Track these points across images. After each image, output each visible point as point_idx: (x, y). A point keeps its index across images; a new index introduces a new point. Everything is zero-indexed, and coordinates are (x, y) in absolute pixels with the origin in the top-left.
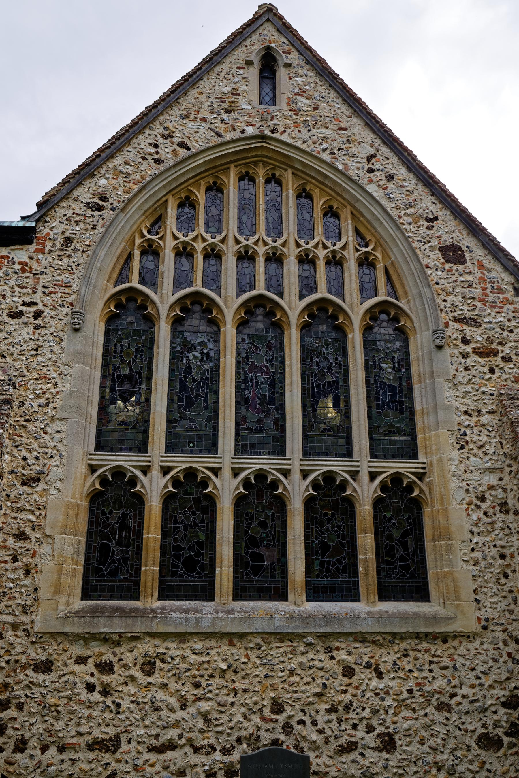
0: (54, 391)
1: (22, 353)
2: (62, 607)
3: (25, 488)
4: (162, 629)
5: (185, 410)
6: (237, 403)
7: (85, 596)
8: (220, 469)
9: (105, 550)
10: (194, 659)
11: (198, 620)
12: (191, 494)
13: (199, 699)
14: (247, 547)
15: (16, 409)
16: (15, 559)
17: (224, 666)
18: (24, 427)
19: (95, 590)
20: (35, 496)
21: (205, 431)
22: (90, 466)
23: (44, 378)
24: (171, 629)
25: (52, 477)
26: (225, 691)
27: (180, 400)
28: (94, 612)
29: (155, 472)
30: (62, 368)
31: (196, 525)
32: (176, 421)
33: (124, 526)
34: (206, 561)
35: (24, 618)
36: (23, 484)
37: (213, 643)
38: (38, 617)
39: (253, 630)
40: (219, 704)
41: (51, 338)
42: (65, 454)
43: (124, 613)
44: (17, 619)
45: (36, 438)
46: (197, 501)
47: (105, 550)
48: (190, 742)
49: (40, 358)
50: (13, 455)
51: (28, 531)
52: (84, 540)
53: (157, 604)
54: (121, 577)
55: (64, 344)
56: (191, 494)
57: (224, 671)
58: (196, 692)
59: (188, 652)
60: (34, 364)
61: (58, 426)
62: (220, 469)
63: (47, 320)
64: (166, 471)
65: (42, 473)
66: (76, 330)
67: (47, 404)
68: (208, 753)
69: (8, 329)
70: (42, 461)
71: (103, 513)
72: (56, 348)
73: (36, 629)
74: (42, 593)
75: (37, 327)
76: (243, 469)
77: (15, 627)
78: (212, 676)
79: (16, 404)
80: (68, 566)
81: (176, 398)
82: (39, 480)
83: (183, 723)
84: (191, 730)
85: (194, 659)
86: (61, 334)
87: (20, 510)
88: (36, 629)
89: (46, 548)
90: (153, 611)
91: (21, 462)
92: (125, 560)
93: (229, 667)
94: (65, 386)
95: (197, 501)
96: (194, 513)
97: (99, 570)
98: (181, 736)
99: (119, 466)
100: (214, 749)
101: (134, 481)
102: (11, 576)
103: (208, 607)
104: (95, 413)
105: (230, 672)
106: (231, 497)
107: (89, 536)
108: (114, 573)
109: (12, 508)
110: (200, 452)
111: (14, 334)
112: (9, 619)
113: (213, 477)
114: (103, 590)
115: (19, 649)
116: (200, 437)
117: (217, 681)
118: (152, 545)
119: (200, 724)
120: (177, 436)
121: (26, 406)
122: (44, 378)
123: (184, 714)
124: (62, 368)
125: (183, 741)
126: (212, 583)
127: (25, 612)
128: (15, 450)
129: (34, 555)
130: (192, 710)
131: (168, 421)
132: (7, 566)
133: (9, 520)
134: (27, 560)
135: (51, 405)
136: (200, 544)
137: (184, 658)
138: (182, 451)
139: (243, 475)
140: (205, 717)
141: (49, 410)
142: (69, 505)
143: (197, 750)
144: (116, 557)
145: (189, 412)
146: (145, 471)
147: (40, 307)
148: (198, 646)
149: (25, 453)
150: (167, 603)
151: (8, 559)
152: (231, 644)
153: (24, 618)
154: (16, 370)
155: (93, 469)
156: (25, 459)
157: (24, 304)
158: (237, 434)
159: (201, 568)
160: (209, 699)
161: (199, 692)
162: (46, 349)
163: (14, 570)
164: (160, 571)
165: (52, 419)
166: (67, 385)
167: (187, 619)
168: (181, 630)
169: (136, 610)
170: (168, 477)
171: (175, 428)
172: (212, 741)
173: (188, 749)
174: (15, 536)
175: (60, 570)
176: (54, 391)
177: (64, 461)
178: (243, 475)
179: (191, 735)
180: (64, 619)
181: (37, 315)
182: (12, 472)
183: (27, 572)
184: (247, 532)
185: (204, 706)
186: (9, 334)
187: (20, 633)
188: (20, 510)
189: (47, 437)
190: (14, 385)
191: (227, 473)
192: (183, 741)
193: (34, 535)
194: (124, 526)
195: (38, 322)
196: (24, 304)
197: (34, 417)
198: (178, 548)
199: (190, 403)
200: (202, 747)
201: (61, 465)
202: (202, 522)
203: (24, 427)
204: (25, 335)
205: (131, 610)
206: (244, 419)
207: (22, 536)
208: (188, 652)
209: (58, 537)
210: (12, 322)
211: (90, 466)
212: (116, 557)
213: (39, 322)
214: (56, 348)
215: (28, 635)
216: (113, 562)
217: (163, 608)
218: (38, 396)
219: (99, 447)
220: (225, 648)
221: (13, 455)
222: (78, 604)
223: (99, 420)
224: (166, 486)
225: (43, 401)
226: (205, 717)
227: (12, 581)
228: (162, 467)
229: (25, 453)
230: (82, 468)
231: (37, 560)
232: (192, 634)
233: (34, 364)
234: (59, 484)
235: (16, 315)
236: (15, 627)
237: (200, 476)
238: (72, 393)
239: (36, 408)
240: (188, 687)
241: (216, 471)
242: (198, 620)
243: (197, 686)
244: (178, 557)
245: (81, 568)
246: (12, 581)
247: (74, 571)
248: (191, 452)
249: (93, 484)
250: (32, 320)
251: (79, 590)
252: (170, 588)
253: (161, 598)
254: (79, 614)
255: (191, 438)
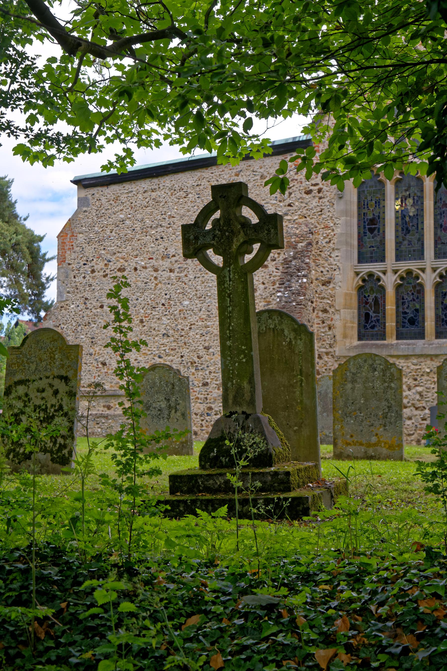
0: (332, 233)
1: (314, 214)
2: (347, 344)
3: (324, 287)
4: (396, 353)
5: (405, 235)
6: (435, 228)
7: (360, 339)
8: (425, 268)
9: (367, 316)
10: (413, 367)
11: (414, 348)
12: (410, 283)
13: (416, 386)
14: (443, 310)
15: (315, 246)
16: (323, 322)
17: (428, 370)
18: (320, 255)
19: (364, 336)
20: (329, 291)
21: (417, 247)
22: (356, 272)
23: (326, 227)
24: (401, 353)
25: (336, 280)
26: (429, 382)
27: (403, 229)
28: (363, 346)
29: (389, 273)
30: (336, 220)
31: (414, 300)
32: (401, 243)
33: (376, 301)
34: (420, 319)
35: (331, 350)
36: (323, 285)
37: (422, 359)
38: (337, 349)
39: (442, 352)
40: (427, 388)
41: (328, 204)
42: (341, 268)
43: (377, 346)
44: (328, 351)
45: (326, 261)
46: (414, 287)
47: (367, 316)
48: (413, 405)
49: (323, 216)
50: (316, 271)
51: (328, 308)
52: (356, 311)
53: (395, 342)
54: (376, 329)
55: (335, 206)
56: (410, 283)
57: (428, 373)
58: (415, 382)
59: (410, 364)
60: (321, 220)
61: (336, 253)
62: (425, 268)
63: (325, 193)
64: (395, 272)
65: (331, 278)
66: (341, 198)
67: (330, 241)
68: (422, 410)
69: (306, 201)
70: (330, 273)
71: (365, 297)
72: (331, 209)
73: (337, 354)
74: (338, 338)
75: (320, 198)
76: (438, 268)
77: (327, 354)
78: (422, 375)
79: (314, 244)
80: (349, 325)
81: (400, 229)
82: (330, 282)
83: (409, 397)
84: (413, 400)
85: (413, 367)
86: (333, 200)
87: (323, 298)
88: (337, 354)
89: (337, 317)
90: (392, 345)
91: (320, 274)
92: (378, 320)
93: (431, 371)
94: (338, 231)
95: (414, 287)
96: (413, 294)
97: (365, 326)
98: (408, 402)
99: (370, 271)
100: (424, 408)
101: (379, 279)
102: (323, 330)
103: (420, 342)
104: (356, 243)
105: (432, 373)
106: (432, 284)
107: (359, 308)
108: (373, 327)
109: (319, 298)
110: (415, 259)
111: (309, 204)
112: (324, 350)
113: (421, 274)
114: (368, 336)
115: (330, 364)
116: (414, 251)
117: (425, 378)
118: (390, 312)
119: (418, 397)
120: (401, 251)
121: (320, 243)
122: (326, 227)
123: (410, 393)
124: (336, 220)
125: (410, 404)
126: (424, 330)
127: (331, 347)
128: (317, 268)
129: (332, 320)
130: (414, 391)
131: (397, 243)
132: (320, 326)
133: (318, 303)
134: (329, 322)
135: (332, 242)
136: (417, 310)
137: (408, 367)
138: (405, 260)
139: (438, 271)
140: (420, 394)
141: (331, 245)
142: (346, 294)
143: (417, 409)
144: (373, 319)
145: (408, 237)
146: (384, 273)
147: (321, 186)
148: (415, 361)
149: (322, 269)
150: (400, 341)
151: (320, 322)
152: (432, 360)
153: (331, 350)
154: (312, 224)
155: (357, 274)
156: (322, 272)
157: (313, 185)
158: (436, 246)
159: (418, 323)
160: (421, 386)
161: (417, 383)
162: (326, 210)
163: (324, 327)
164: (397, 325)
165: (333, 249)
166: (339, 230)
167: (408, 348)
168: (406, 353)
169: (384, 345)
170: (397, 275)
171: (400, 246)
172: (424, 405)
173: (412, 408)
174: (322, 311)
175: (345, 327)
176: (332, 233)
177: (341, 272)
178: (438, 271)
179: (413, 402)
180: (349, 350)
181: (320, 191)
182: (317, 279)
183: (330, 328)
184: (442, 303)
185: (419, 389)
186: (307, 204)
187: (330, 357)
188: (323, 298)
189: (331, 259)
190: (312, 233)
191: (429, 270)
192: (410, 404)
193: (331, 310)
194: (376, 301)
195: (321, 195)
196: (313, 185)
197: (325, 249)
198: (405, 313)
199: (408, 231)
200: (419, 407)
201: (340, 274)
202: (418, 298)
203: (320, 255)
204: (314, 204)
205: (381, 345)
206: (439, 238)
207: (325, 311)
208: (410, 364)
209: (342, 311)
210: (307, 196)
211: (356, 272)
212: (373, 319)
213: (321, 195)
214: (331, 209)
215: (333, 357)
216: (372, 322)
217: (397, 344)
218: (325, 238)
219: (360, 261)
220: (429, 362)
221: (316, 271)
222: (356, 342)
223: (359, 245)
224: (396, 280)
225: (327, 240)
226: (420, 394)
227: (323, 333)
228: (393, 270)
229: (322, 269)
230: (352, 274)
231: (333, 322)
232: (411, 355)
233: (321, 220)
234: (340, 284)
235: (308, 192)
236: (327, 354)
237: (414, 273)
238: (341, 234)
239: (325, 244)
240: (411, 380)
241: (423, 270)
242: (414, 348)
243: (416, 380)
244: (405, 318)
245: (356, 325)
246: (323, 333)
247: (352, 327)
248: (410, 260)
249: (358, 282)
250: (317, 194)
251: (356, 336)
252: (402, 334)
253: (397, 338)
254: (356, 347)
255: (410, 251)
